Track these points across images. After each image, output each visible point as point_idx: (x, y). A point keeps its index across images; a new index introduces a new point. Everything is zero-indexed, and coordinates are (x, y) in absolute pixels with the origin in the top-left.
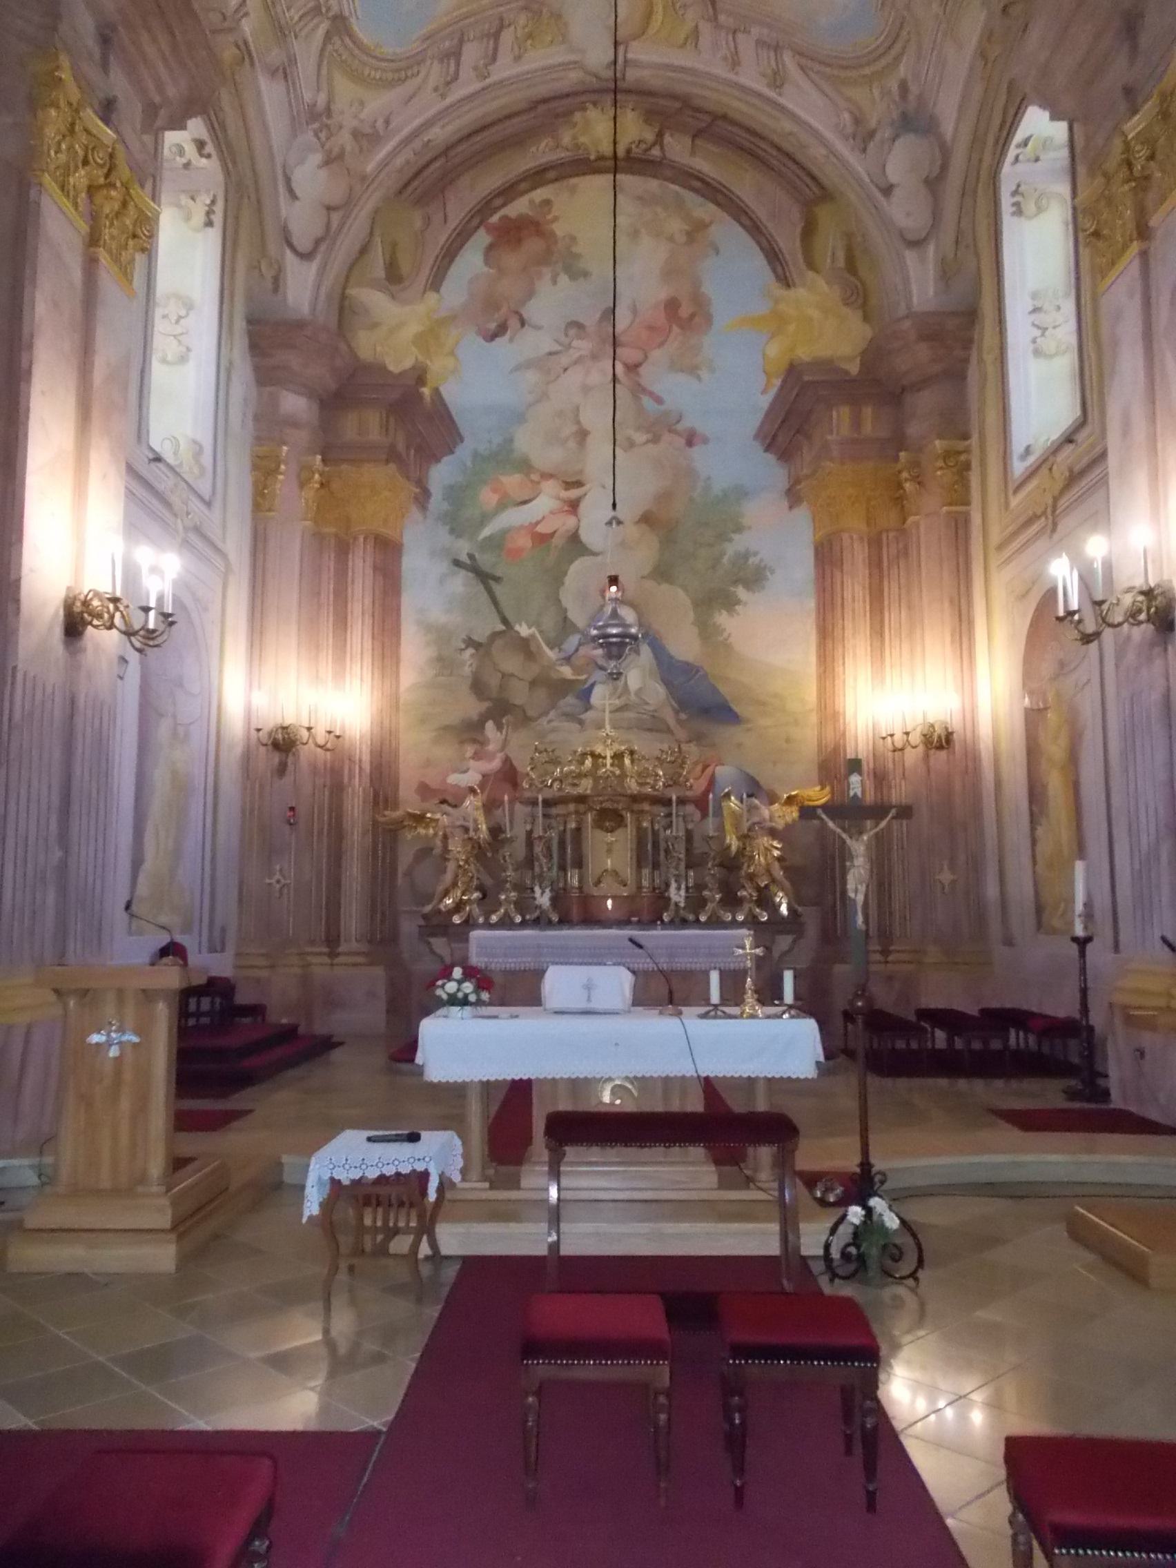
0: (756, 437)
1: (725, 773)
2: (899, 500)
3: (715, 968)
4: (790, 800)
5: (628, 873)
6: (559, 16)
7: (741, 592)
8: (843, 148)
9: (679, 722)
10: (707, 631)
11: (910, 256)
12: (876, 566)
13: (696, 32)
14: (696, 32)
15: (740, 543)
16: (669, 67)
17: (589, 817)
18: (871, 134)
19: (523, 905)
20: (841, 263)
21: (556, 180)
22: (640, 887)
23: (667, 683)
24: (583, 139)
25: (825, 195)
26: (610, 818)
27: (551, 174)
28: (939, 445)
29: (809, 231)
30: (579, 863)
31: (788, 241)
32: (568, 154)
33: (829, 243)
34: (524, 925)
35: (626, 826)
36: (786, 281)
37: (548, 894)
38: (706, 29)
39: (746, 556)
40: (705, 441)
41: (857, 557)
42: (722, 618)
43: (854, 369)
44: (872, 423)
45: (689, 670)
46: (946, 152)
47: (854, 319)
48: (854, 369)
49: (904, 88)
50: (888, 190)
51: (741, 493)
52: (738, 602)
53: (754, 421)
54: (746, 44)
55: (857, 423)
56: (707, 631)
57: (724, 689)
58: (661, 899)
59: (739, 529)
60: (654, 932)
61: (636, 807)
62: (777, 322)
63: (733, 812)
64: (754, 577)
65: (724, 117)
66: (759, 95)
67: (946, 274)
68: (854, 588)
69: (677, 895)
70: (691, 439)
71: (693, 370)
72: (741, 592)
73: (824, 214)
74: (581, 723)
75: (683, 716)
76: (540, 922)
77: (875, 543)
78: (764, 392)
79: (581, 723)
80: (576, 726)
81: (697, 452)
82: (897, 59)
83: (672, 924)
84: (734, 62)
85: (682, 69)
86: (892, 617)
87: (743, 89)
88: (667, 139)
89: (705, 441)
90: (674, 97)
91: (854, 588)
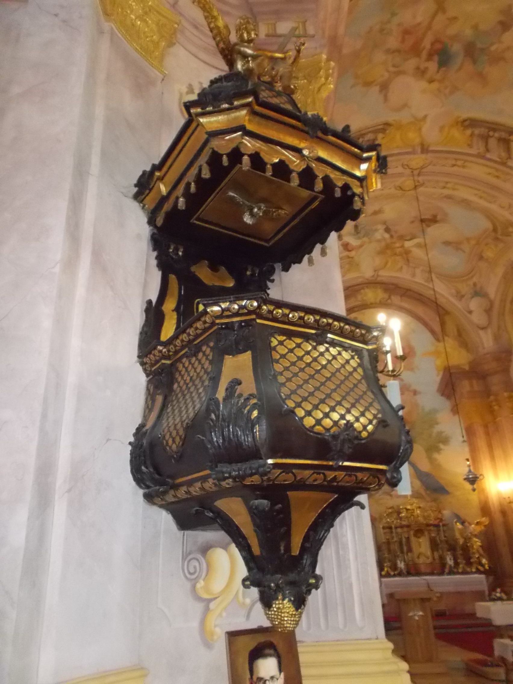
0: (438, 391)
1: (446, 513)
2: (492, 412)
3: (435, 601)
4: (478, 523)
5: (429, 553)
6: (358, 265)
7: (442, 446)
8: (453, 300)
9: (426, 494)
10: (432, 460)
11: (481, 332)
12: (487, 434)
13: (401, 268)
14: (401, 268)
15: (437, 428)
16: (391, 277)
17: (412, 533)
18: (463, 296)
19: (394, 567)
20: (456, 333)
21: (358, 311)
22: (434, 559)
23: (421, 481)
24: (365, 298)
25: (447, 313)
26: (419, 532)
27: (356, 309)
28: (506, 394)
29: (443, 324)
30: (410, 550)
31: (437, 328)
32: (360, 303)
33: (451, 327)
34: (394, 576)
35: (425, 536)
36: (438, 340)
37: (403, 563)
38: (405, 267)
39: (441, 433)
40: (420, 393)
41: (480, 432)
42: (436, 456)
43: (467, 368)
44: (477, 386)
45: (428, 475)
46: (492, 303)
47: (464, 352)
48: (467, 368)
49: (475, 284)
50: (470, 312)
51: (435, 411)
52: (441, 449)
53: (435, 386)
54: (418, 271)
55: (472, 386)
56: (432, 460)
57: (442, 482)
58: (443, 565)
59: (437, 423)
60: (444, 577)
61: (428, 528)
62: (437, 353)
63: (459, 529)
64: (445, 441)
65: (410, 290)
66: (422, 284)
67: (497, 338)
68: (481, 443)
69: (450, 562)
70: (415, 393)
71: (412, 370)
72: (442, 446)
73: (447, 318)
74: (391, 496)
75: (428, 492)
76: (400, 574)
77: (486, 426)
78: (438, 376)
79: (391, 496)
80: (388, 497)
81: (418, 397)
82: (472, 277)
83: (450, 573)
84: (414, 275)
85: (395, 277)
86: (498, 452)
87: (416, 283)
88: (393, 297)
89: (420, 393)
90: (393, 284)
91: (481, 443)
